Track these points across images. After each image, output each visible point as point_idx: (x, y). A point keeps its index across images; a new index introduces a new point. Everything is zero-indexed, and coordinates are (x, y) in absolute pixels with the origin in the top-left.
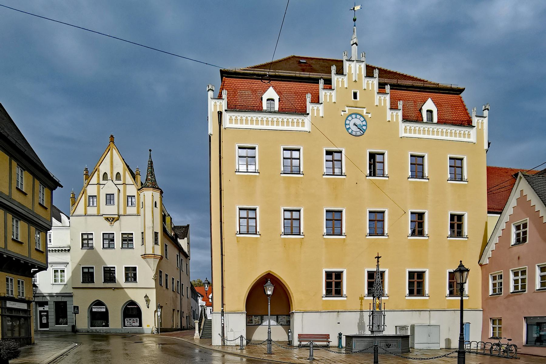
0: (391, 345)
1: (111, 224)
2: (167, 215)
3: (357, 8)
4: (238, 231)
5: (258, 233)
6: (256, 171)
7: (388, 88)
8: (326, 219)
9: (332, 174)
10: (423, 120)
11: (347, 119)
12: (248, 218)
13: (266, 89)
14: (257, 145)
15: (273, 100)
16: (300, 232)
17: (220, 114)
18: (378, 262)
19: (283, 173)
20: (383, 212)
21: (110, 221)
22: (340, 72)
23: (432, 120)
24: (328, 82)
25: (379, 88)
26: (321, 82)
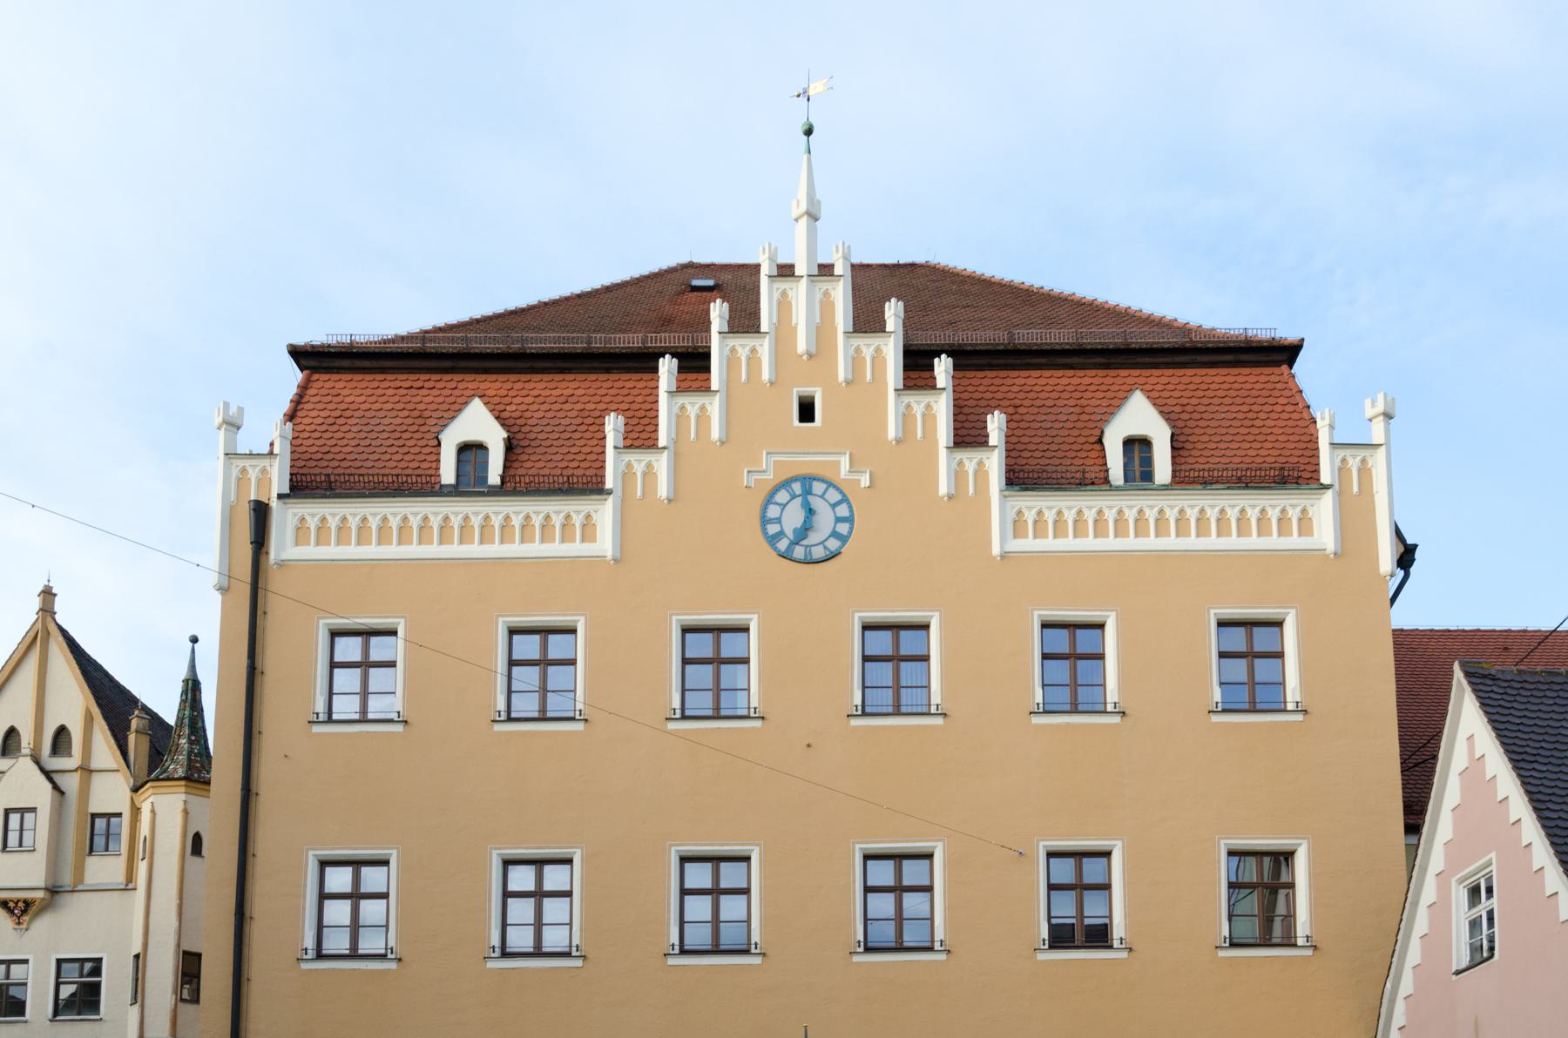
1: (19, 923)
3: (815, 88)
4: (677, 942)
5: (753, 946)
6: (752, 715)
7: (943, 367)
9: (710, 713)
10: (1106, 481)
11: (769, 500)
13: (1115, 402)
14: (402, 621)
16: (933, 941)
17: (261, 512)
19: (1220, 709)
20: (1107, 854)
21: (16, 911)
22: (745, 321)
23: (1148, 476)
24: (695, 362)
25: (907, 367)
26: (667, 366)
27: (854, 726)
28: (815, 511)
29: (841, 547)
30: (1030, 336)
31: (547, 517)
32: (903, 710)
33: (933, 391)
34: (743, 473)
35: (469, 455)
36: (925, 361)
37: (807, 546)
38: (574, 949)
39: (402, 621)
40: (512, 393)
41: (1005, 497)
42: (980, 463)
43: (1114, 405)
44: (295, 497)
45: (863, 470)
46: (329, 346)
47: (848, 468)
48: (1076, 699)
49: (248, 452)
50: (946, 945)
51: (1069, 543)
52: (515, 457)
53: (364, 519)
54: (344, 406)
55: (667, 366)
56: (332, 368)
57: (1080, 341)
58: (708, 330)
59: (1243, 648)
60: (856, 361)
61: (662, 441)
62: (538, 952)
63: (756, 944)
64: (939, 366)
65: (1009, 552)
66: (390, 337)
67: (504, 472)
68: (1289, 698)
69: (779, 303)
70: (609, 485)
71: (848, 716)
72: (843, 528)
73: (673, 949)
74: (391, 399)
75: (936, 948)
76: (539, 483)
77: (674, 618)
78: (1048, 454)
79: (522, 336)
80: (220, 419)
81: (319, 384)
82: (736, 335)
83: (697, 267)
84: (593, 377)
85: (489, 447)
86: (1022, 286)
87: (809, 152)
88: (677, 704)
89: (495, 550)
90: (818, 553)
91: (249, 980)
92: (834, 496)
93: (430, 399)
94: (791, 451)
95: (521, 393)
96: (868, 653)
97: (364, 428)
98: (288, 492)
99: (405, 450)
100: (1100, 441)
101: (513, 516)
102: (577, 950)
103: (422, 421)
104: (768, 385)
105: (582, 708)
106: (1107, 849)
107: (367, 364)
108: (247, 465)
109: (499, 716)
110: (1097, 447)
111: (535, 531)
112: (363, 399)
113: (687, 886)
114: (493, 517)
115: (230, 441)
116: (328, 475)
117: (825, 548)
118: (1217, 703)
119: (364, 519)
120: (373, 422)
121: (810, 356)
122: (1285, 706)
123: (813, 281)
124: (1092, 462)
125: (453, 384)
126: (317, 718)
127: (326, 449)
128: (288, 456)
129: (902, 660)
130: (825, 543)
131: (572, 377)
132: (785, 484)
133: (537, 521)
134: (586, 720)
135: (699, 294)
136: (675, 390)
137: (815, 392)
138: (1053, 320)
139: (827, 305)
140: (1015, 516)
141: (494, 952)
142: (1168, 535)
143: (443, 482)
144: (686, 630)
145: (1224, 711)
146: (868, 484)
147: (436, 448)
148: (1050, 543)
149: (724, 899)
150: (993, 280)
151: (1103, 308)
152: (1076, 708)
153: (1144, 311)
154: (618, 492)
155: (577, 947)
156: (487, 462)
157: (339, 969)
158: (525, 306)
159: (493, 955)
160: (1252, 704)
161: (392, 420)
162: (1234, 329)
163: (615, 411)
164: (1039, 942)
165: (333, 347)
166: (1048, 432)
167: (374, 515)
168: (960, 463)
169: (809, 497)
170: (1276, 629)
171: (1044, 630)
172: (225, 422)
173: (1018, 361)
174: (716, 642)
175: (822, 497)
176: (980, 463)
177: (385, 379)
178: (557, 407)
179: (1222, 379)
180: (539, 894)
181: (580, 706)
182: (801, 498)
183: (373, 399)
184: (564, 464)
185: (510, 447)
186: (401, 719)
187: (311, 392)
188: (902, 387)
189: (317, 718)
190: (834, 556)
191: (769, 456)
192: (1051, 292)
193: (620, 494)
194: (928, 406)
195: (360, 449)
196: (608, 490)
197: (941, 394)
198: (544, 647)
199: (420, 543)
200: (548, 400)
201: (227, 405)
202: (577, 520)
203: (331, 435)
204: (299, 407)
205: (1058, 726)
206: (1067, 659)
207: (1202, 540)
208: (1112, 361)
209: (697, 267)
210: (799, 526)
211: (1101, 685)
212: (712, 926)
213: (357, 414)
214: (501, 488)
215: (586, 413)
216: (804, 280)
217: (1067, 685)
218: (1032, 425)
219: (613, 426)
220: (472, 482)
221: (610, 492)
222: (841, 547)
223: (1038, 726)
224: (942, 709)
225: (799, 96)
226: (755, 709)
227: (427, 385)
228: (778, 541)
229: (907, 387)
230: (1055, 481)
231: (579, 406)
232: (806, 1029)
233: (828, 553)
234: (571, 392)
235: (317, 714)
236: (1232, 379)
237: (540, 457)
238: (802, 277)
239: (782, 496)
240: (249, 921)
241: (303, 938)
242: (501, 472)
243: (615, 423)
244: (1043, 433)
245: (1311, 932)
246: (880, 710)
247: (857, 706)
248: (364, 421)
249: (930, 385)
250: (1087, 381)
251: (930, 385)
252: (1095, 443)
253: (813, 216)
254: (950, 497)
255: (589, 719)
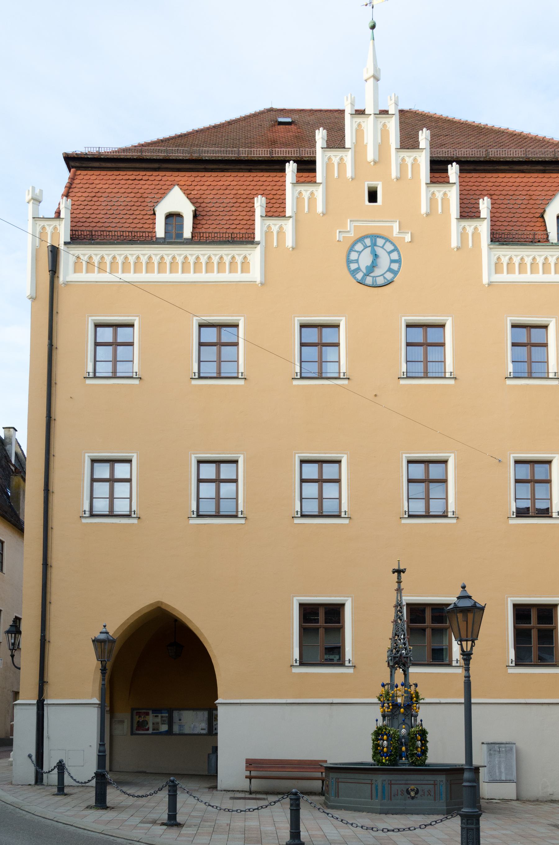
0: (418, 790)
2: (16, 474)
6: (134, 376)
7: (453, 170)
8: (515, 480)
9: (215, 375)
10: (547, 240)
11: (351, 249)
12: (321, 481)
14: (137, 318)
15: (179, 216)
17: (54, 252)
18: (399, 582)
19: (512, 376)
20: (445, 462)
25: (432, 171)
26: (291, 168)
27: (402, 384)
28: (379, 256)
29: (394, 278)
30: (496, 153)
31: (150, 258)
32: (429, 375)
33: (449, 185)
34: (336, 233)
35: (173, 220)
36: (442, 167)
37: (374, 277)
38: (240, 513)
39: (137, 318)
40: (194, 183)
41: (491, 249)
42: (476, 228)
43: (163, 193)
44: (74, 244)
45: (406, 231)
46: (86, 154)
47: (398, 230)
48: (427, 370)
49: (42, 217)
50: (456, 514)
51: (528, 277)
52: (198, 222)
53: (114, 258)
54: (97, 190)
55: (291, 168)
56: (88, 167)
57: (528, 156)
58: (314, 146)
59: (214, 340)
60: (402, 166)
61: (288, 213)
62: (111, 514)
63: (134, 512)
64: (289, 168)
65: (493, 282)
66: (116, 149)
67: (193, 231)
68: (551, 370)
69: (357, 130)
70: (257, 239)
71: (399, 378)
72: (395, 266)
73: (297, 514)
74: (124, 187)
75: (342, 516)
76: (107, 236)
77: (296, 319)
78: (511, 224)
79: (199, 150)
80: (30, 197)
81: (81, 177)
82: (331, 149)
83: (276, 111)
84: (241, 174)
85: (184, 216)
86: (473, 124)
87: (374, 40)
88: (196, 370)
89: (191, 277)
90: (380, 281)
91: (52, 528)
92: (389, 247)
93: (146, 187)
94: (364, 219)
95: (199, 183)
96: (303, 341)
97: (109, 203)
98: (70, 241)
99: (134, 216)
100: (542, 217)
101: (201, 257)
102: (242, 514)
103: (143, 200)
104: (350, 180)
105: (138, 371)
106: (549, 459)
107: (109, 165)
108: (45, 224)
109: (195, 376)
110: (541, 220)
111: (142, 265)
112: (107, 186)
113: (201, 477)
114: (177, 257)
115: (35, 210)
116: (91, 231)
117: (384, 278)
118: (510, 373)
119: (114, 258)
120: (114, 200)
121: (375, 163)
122: (548, 375)
123: (376, 117)
124: (538, 228)
125: (159, 178)
126: (89, 375)
127: (88, 216)
128: (69, 220)
129: (324, 346)
130: (384, 275)
131: (229, 174)
132: (361, 239)
133: (203, 260)
134: (245, 379)
135: (284, 126)
136: (295, 182)
137: (378, 184)
138: (502, 144)
139: (385, 132)
140: (496, 260)
141: (193, 514)
142: (526, 273)
143: (157, 236)
144: (302, 326)
145: (515, 378)
146: (410, 240)
147: (152, 216)
148: (516, 277)
149: (116, 485)
150: (454, 120)
151: (528, 137)
152: (427, 375)
153: (554, 139)
154: (263, 243)
155: (242, 512)
156: (183, 224)
157: (105, 523)
158: (186, 132)
159: (193, 516)
160: (320, 374)
161: (125, 199)
162: (115, 148)
163: (261, 195)
164: (510, 513)
165: (89, 155)
166: (511, 210)
167: (120, 255)
168: (464, 228)
169: (375, 247)
170: (544, 330)
171: (408, 329)
172: (33, 199)
173: (491, 168)
174: (218, 333)
175: (382, 247)
176: (476, 228)
177: (119, 174)
178: (221, 192)
179: (534, 180)
180: (112, 480)
181: (136, 369)
182: (370, 248)
183: (113, 186)
184: (227, 226)
185: (195, 216)
186: (137, 377)
187: (76, 181)
188: (429, 182)
189: (89, 375)
190: (390, 282)
191: (352, 222)
192: (493, 128)
193: (264, 244)
194: (445, 194)
195: (108, 216)
196: (256, 241)
197: (452, 186)
198: (115, 335)
199: (147, 272)
200: (215, 188)
201: (33, 188)
202: (239, 260)
203: (90, 207)
204: (71, 190)
205: (521, 386)
206: (525, 346)
207: (546, 275)
208: (547, 168)
209: (276, 111)
210: (369, 265)
211: (132, 361)
212: (216, 501)
213: (104, 195)
214: (192, 240)
215: (238, 196)
216: (372, 116)
217: (111, 361)
218: (501, 206)
219: (259, 203)
220: (174, 237)
221: (258, 243)
222: (394, 278)
223: (509, 386)
224: (454, 375)
225: (366, 5)
226: (242, 373)
227: (144, 178)
228: (357, 274)
229: (432, 182)
230: (517, 240)
231: (234, 192)
232: (399, 563)
233: (386, 281)
234: (229, 183)
235: (89, 373)
236: (540, 180)
237: (213, 222)
238: (371, 115)
239: (359, 247)
240: (51, 494)
241: (83, 504)
242: (191, 231)
243: (66, 204)
244: (508, 211)
245: (455, 509)
246: (417, 375)
247: (195, 373)
248: (109, 199)
249: (446, 181)
250: (532, 180)
251: (446, 181)
252: (539, 217)
253: (376, 78)
254: (458, 249)
255: (247, 378)
